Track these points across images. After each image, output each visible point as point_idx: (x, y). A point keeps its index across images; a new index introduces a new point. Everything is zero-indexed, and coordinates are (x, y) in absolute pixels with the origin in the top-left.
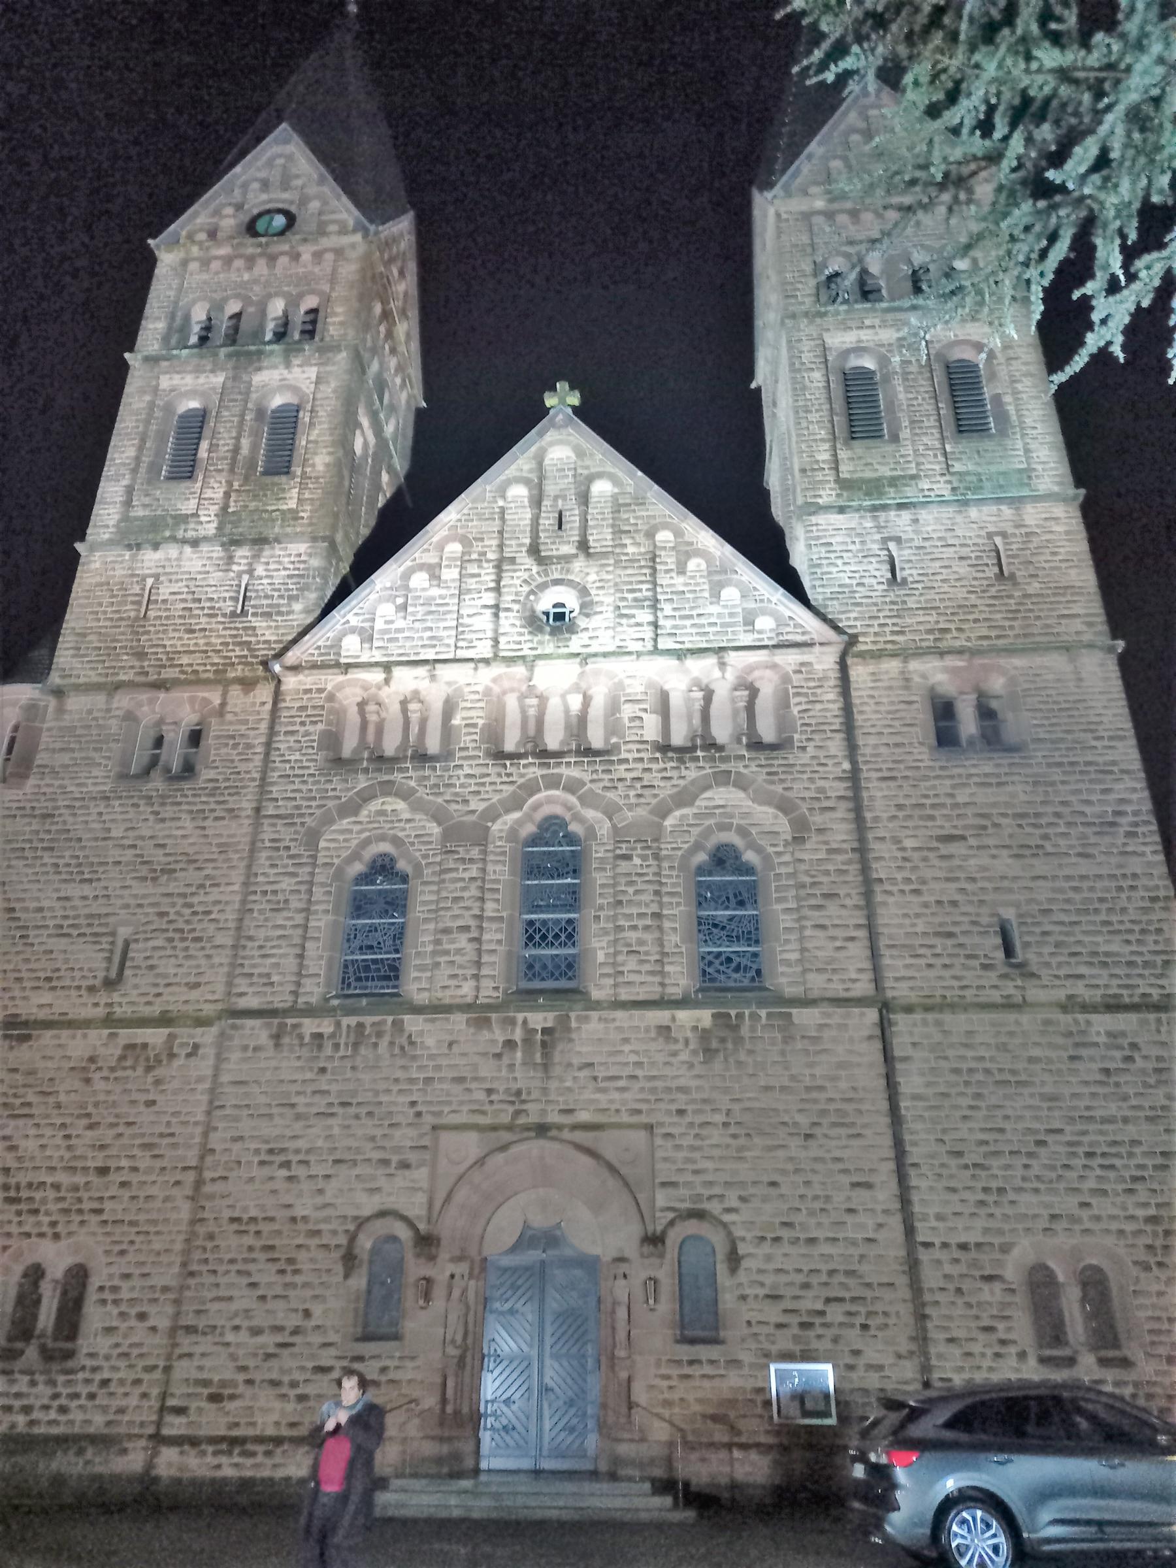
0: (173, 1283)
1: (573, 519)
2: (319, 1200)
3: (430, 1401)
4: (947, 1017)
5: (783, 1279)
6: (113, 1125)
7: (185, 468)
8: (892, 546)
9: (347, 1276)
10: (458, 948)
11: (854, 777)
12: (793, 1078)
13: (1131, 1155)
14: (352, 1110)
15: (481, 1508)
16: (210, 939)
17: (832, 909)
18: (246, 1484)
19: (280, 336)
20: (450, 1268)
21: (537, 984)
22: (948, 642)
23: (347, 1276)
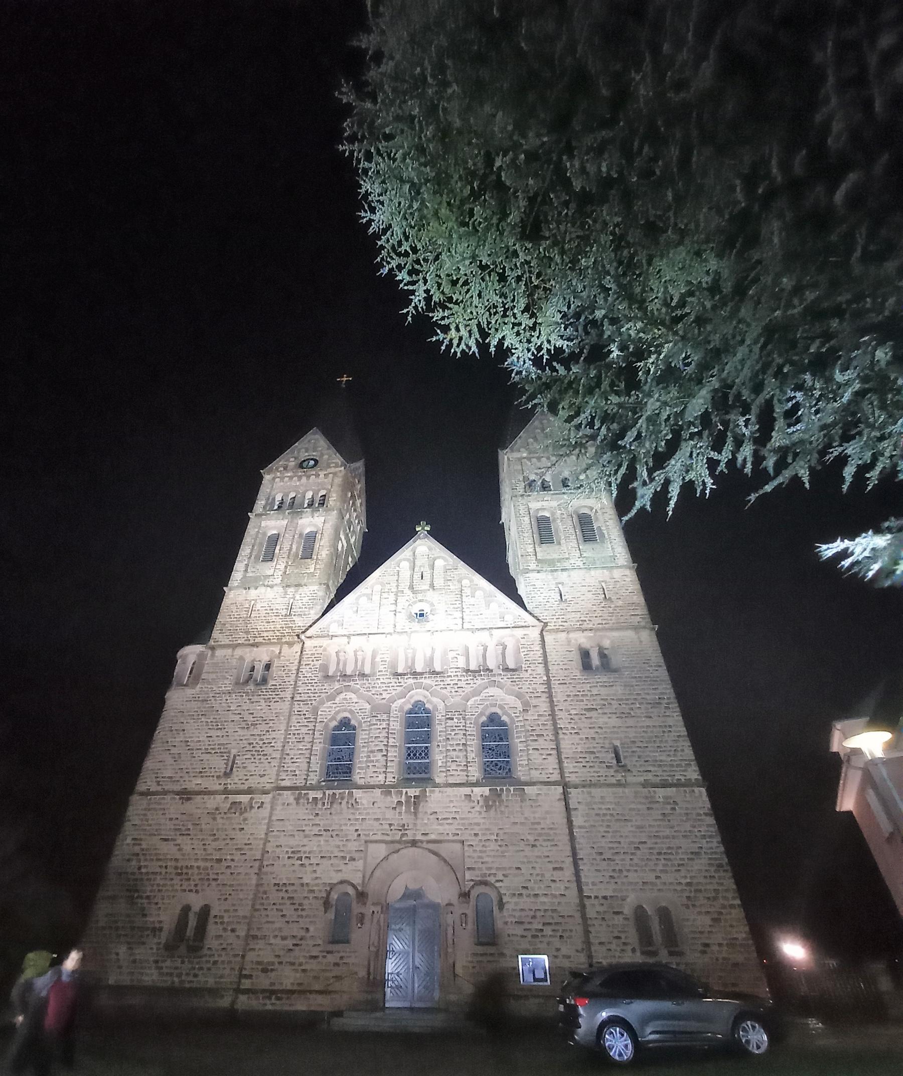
0: (248, 915)
1: (427, 576)
2: (315, 875)
3: (362, 973)
4: (593, 790)
5: (523, 914)
6: (224, 839)
7: (269, 556)
8: (560, 586)
9: (325, 912)
10: (377, 758)
11: (548, 683)
12: (526, 818)
13: (677, 853)
14: (329, 833)
15: (385, 1026)
16: (270, 755)
17: (541, 740)
18: (275, 1013)
19: (311, 505)
20: (373, 908)
21: (412, 776)
22: (585, 626)
23: (325, 912)
